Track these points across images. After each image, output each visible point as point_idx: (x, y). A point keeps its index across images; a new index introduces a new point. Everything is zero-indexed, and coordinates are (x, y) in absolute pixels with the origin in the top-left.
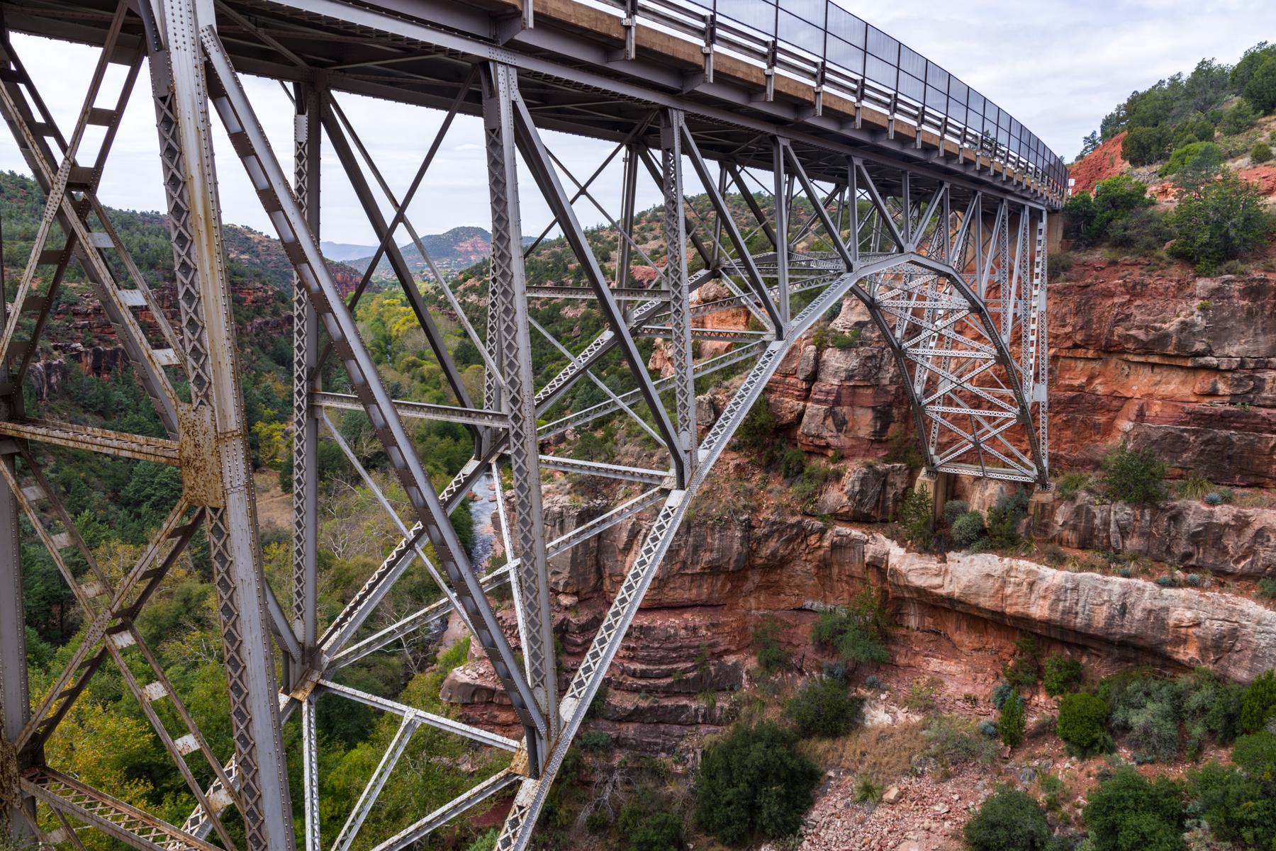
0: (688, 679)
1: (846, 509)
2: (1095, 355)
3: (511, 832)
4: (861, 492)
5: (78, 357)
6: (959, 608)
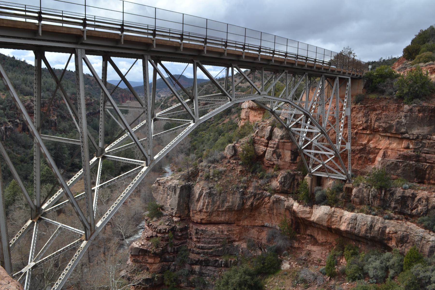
0: (219, 250)
1: (279, 188)
2: (370, 133)
3: (78, 253)
4: (284, 182)
5: (17, 125)
6: (317, 226)
